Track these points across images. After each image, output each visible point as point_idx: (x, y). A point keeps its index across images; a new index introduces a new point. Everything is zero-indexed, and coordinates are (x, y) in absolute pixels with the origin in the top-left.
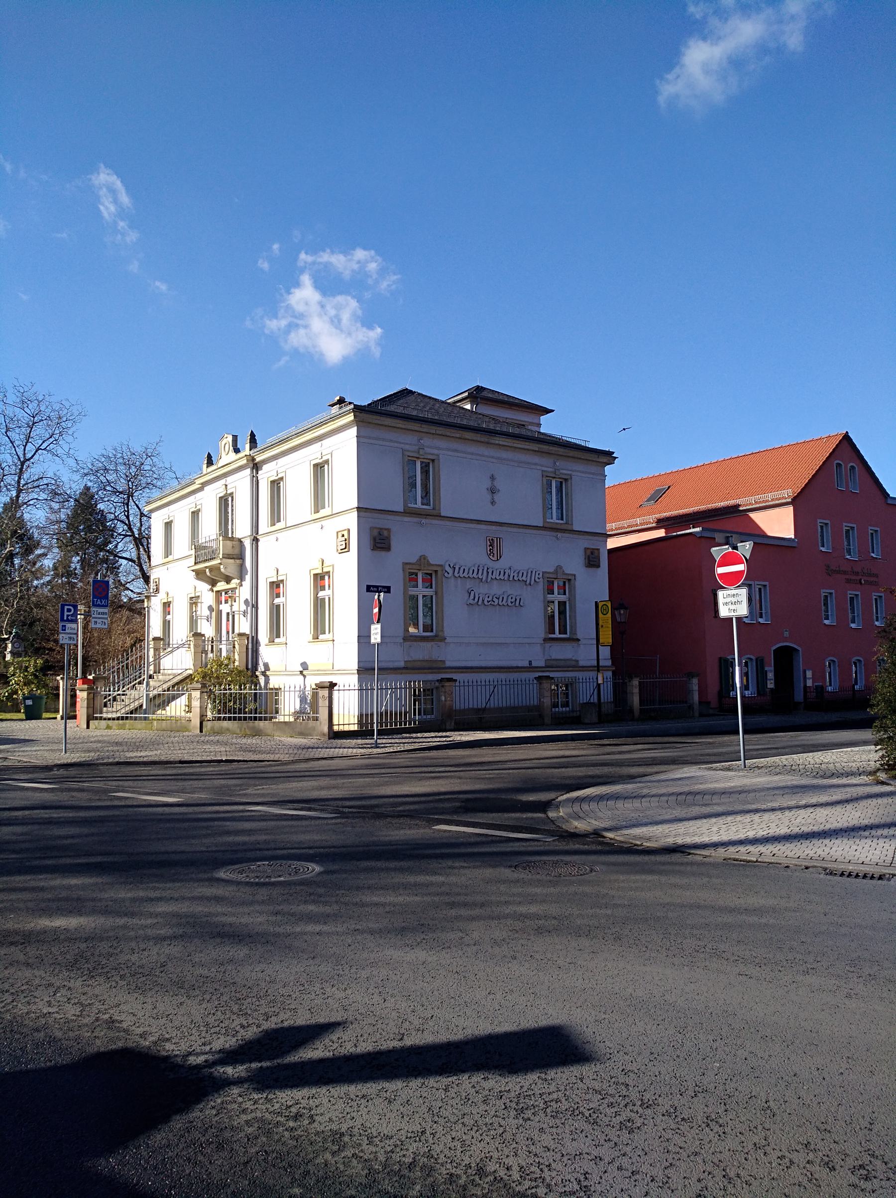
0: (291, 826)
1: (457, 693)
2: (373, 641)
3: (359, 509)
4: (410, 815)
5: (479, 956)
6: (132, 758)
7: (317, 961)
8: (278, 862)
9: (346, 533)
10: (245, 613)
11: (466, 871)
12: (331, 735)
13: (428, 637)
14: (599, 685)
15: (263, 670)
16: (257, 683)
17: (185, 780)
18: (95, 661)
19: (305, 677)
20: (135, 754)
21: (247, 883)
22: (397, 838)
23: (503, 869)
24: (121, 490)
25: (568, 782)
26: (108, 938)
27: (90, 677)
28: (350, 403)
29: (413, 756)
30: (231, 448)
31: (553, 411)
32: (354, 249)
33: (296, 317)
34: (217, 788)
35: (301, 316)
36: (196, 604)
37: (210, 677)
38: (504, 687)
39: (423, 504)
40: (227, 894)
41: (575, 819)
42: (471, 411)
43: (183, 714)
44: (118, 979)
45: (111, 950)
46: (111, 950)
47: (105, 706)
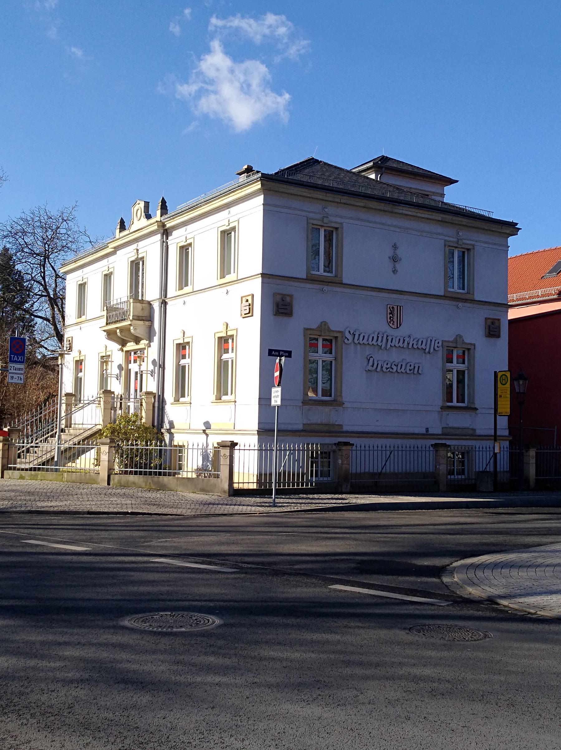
0: (191, 579)
1: (354, 456)
2: (273, 403)
3: (263, 275)
4: (307, 574)
5: (374, 714)
6: (43, 507)
7: (216, 711)
8: (180, 612)
9: (250, 298)
10: (152, 373)
11: (362, 631)
12: (232, 492)
13: (326, 401)
14: (495, 455)
15: (168, 427)
16: (162, 440)
17: (93, 530)
18: (11, 414)
19: (207, 435)
20: (45, 504)
21: (151, 632)
22: (294, 595)
23: (397, 631)
24: (38, 252)
25: (463, 548)
26: (20, 678)
27: (6, 429)
28: (258, 172)
29: (314, 516)
30: (143, 214)
31: (457, 181)
32: (265, 15)
33: (206, 83)
34: (122, 539)
35: (212, 82)
36: (107, 362)
37: (118, 433)
38: (400, 453)
39: (325, 271)
40: (131, 642)
41: (469, 585)
42: (375, 181)
43: (92, 467)
44: (29, 716)
45: (22, 689)
46: (22, 689)
47: (19, 457)
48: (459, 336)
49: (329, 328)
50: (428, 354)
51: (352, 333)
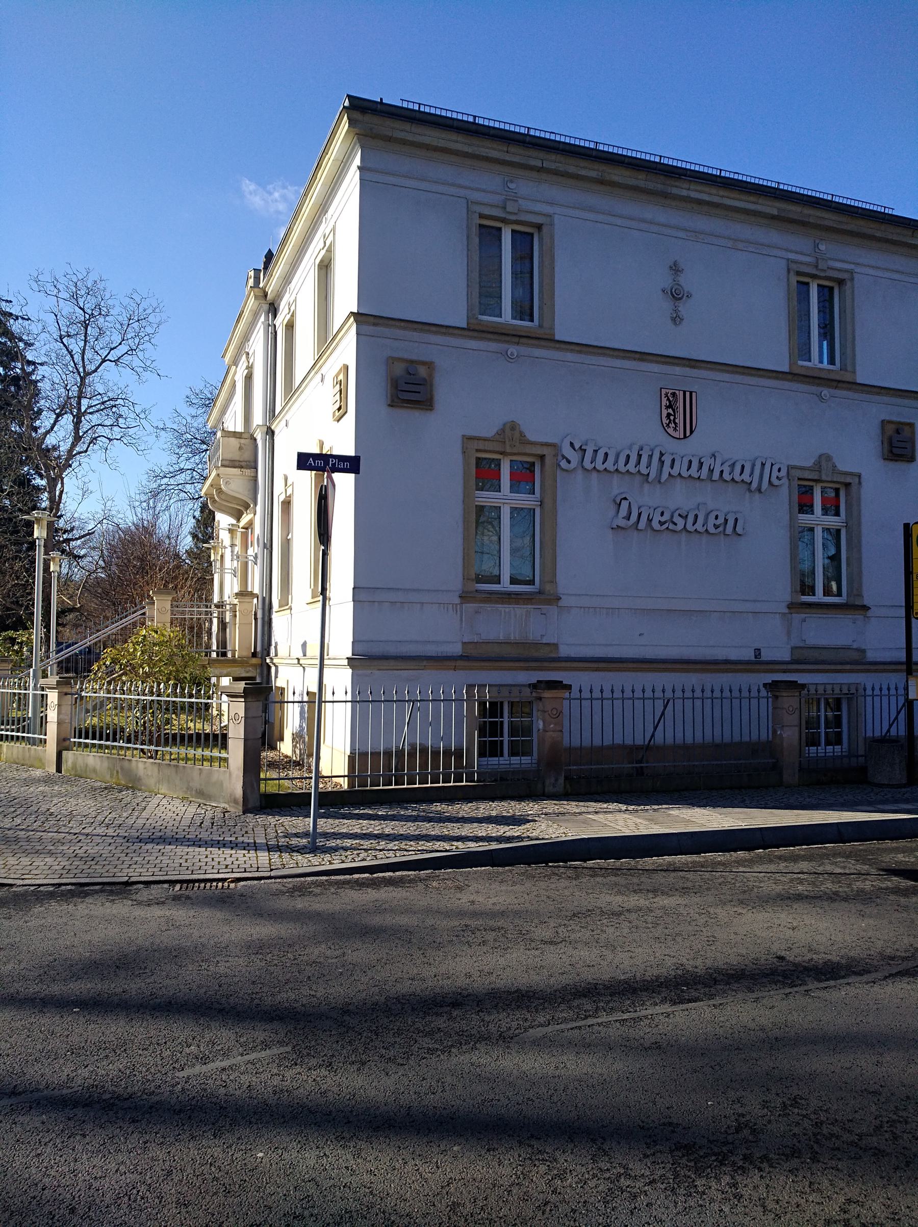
12: (254, 801)
13: (517, 594)
48: (824, 460)
49: (522, 434)
50: (757, 495)
51: (577, 447)
